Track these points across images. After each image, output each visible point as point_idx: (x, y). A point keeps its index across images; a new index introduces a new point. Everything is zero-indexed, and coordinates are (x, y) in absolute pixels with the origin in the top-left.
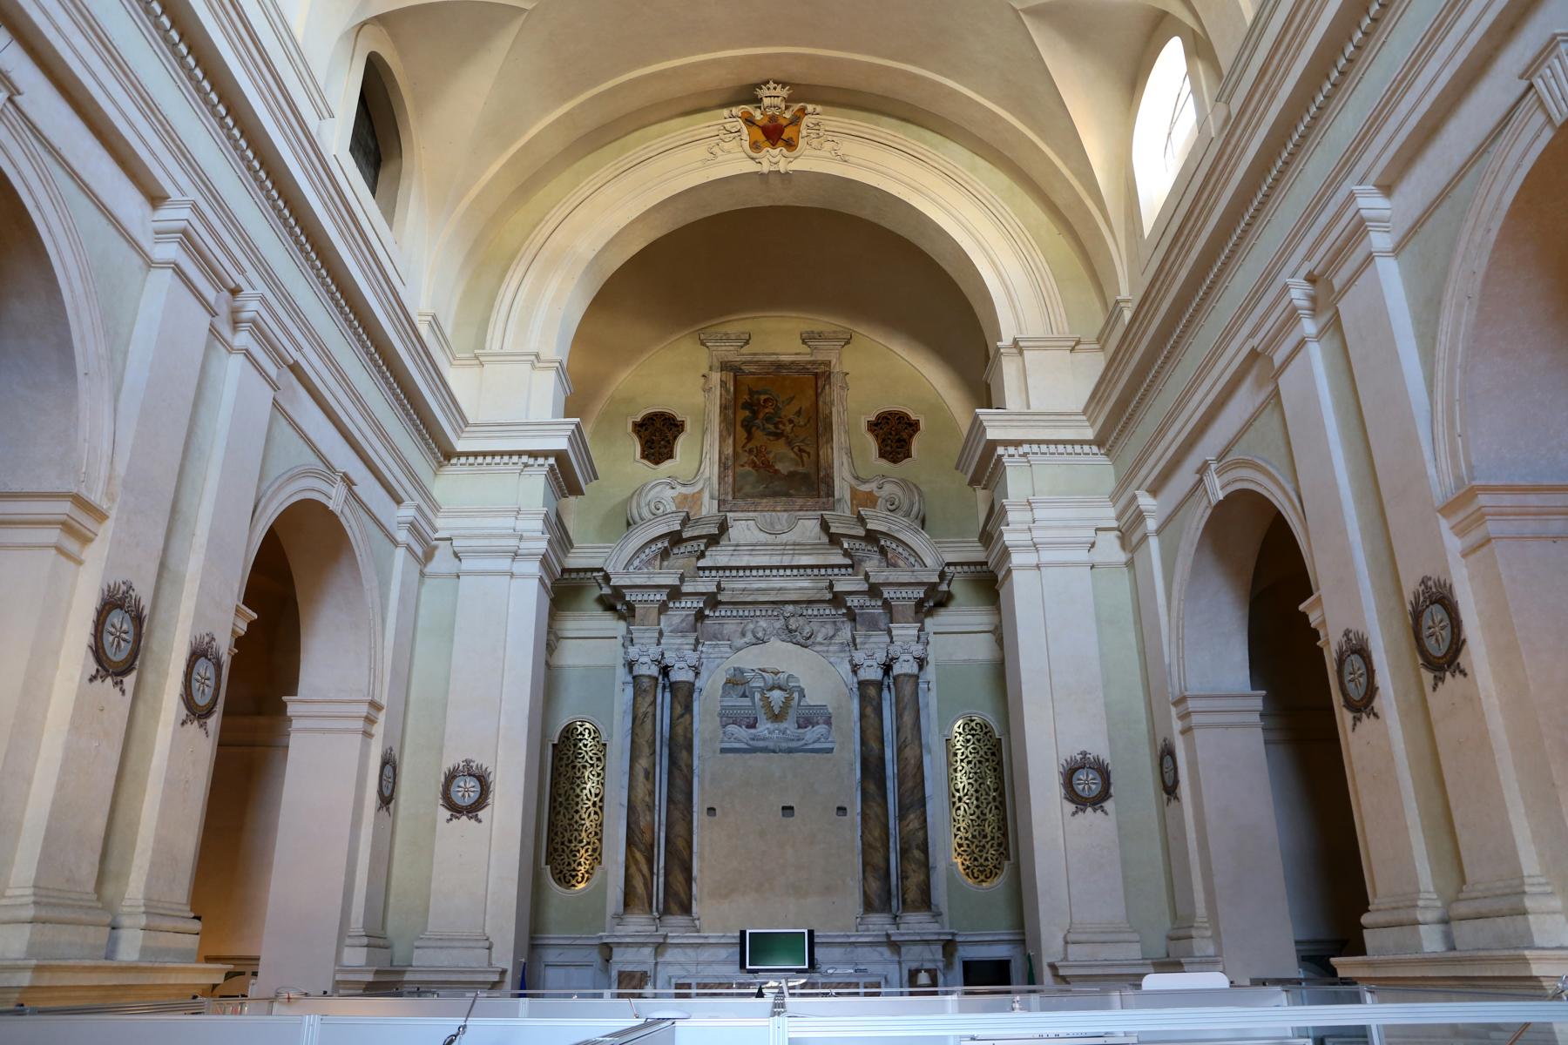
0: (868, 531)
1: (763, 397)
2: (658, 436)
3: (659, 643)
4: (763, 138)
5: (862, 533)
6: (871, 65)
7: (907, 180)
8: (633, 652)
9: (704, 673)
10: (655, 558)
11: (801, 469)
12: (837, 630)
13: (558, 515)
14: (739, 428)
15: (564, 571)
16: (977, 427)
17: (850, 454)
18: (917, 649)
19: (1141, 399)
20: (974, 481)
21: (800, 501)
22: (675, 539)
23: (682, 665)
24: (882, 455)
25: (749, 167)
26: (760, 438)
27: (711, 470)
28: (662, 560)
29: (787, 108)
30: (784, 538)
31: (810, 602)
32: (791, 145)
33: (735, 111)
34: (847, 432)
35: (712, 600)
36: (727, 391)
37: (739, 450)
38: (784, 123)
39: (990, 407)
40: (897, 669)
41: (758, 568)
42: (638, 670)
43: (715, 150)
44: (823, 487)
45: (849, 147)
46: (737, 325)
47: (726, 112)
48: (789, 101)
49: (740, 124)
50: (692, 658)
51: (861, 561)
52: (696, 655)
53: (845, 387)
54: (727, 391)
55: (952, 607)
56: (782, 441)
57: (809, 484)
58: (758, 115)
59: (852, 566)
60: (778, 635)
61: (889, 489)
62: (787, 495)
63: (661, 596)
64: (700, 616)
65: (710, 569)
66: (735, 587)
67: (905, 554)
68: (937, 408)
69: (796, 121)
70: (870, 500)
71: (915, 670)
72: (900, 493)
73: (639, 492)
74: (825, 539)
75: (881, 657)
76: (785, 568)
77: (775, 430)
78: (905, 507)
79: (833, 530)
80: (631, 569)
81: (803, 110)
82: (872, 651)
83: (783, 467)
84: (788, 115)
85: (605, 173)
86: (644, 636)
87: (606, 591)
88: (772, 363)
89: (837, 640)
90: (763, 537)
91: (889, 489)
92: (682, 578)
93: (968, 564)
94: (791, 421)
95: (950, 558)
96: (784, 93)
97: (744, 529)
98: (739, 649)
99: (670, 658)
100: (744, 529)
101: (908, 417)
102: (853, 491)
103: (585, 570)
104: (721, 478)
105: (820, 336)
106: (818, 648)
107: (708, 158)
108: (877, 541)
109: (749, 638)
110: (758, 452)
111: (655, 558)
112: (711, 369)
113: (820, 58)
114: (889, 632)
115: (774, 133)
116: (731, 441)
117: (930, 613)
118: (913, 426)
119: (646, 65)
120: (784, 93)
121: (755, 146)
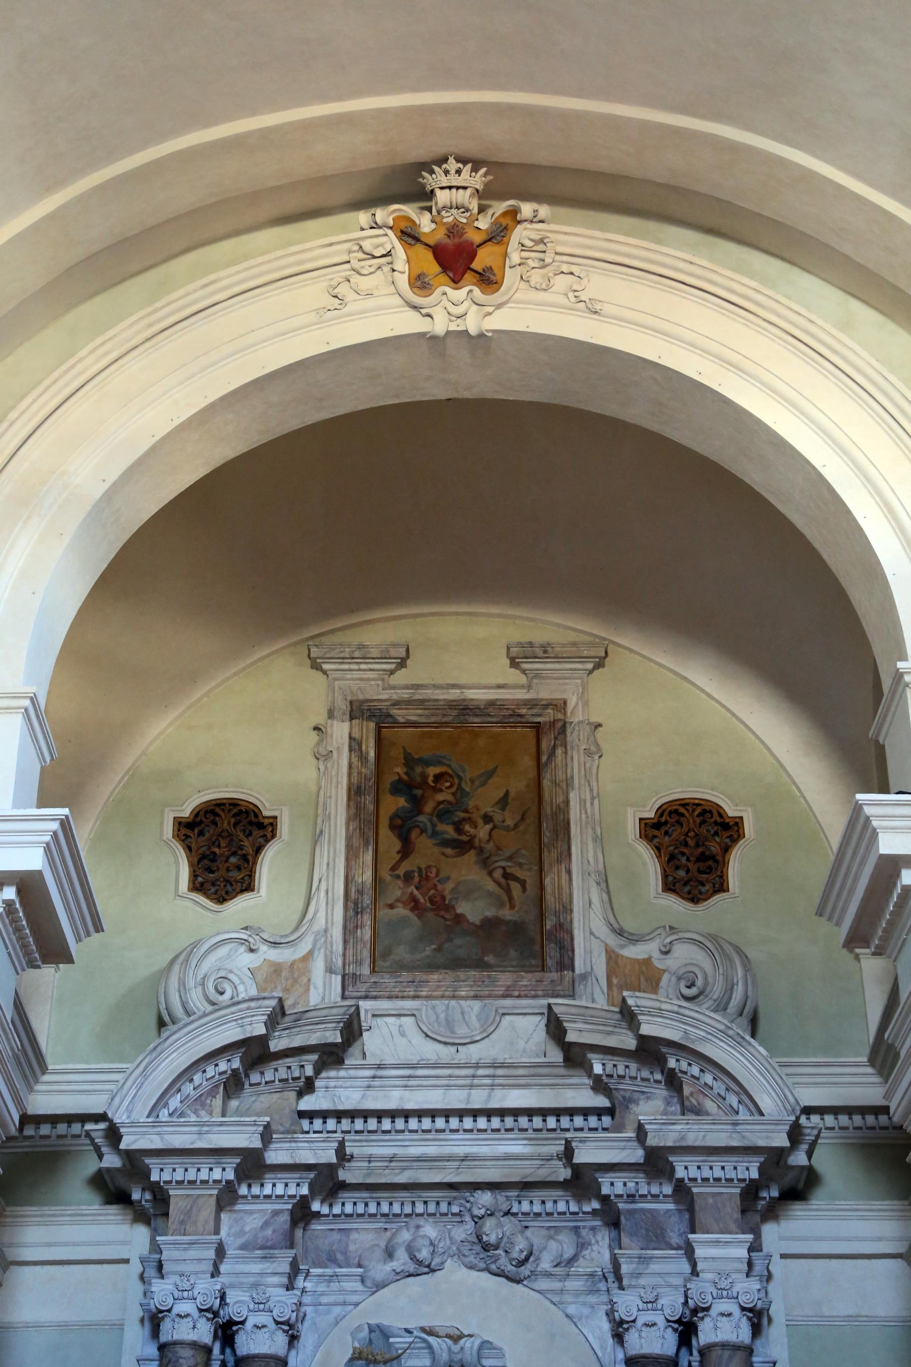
0: (643, 1040)
1: (433, 771)
2: (224, 844)
3: (215, 1273)
4: (435, 268)
5: (631, 1043)
6: (646, 126)
7: (714, 347)
8: (162, 1290)
9: (307, 1338)
10: (212, 1093)
11: (507, 914)
12: (582, 1246)
13: (18, 1006)
14: (385, 831)
15: (26, 1119)
16: (860, 830)
17: (604, 882)
18: (748, 1290)
19: (68, 903)
20: (856, 939)
21: (504, 979)
22: (255, 1053)
23: (263, 1318)
24: (669, 887)
25: (408, 323)
26: (426, 850)
27: (329, 913)
28: (228, 1096)
29: (482, 209)
30: (474, 1052)
31: (526, 1186)
32: (488, 281)
33: (383, 214)
34: (599, 840)
35: (328, 1181)
36: (363, 758)
37: (386, 875)
38: (477, 238)
39: (885, 790)
40: (708, 1332)
41: (420, 1114)
42: (171, 1331)
43: (343, 290)
44: (551, 950)
45: (600, 285)
46: (382, 630)
47: (363, 217)
48: (485, 195)
49: (392, 240)
50: (283, 1303)
51: (629, 1101)
52: (291, 1298)
53: (594, 752)
54: (363, 758)
55: (818, 1201)
56: (471, 857)
57: (523, 942)
58: (425, 224)
59: (610, 1112)
60: (460, 1255)
61: (685, 955)
62: (480, 965)
63: (224, 1172)
64: (302, 1214)
65: (324, 1115)
66: (373, 1152)
67: (719, 1088)
68: (780, 793)
69: (498, 235)
70: (647, 977)
71: (744, 1334)
72: (706, 964)
73: (184, 957)
74: (556, 1056)
75: (672, 1304)
76: (475, 1114)
77: (458, 837)
78: (717, 991)
79: (571, 1037)
80: (164, 1115)
81: (513, 213)
82: (656, 1289)
83: (473, 910)
84: (484, 223)
85: (128, 331)
86: (187, 1256)
87: (112, 1161)
88: (451, 705)
89: (582, 1267)
90: (431, 1051)
91: (685, 955)
92: (267, 1135)
93: (849, 1111)
94: (487, 819)
95: (811, 1096)
96: (478, 180)
97: (393, 1034)
98: (380, 1286)
99: (238, 1304)
100: (393, 1034)
101: (721, 813)
102: (612, 958)
103: (70, 1119)
104: (349, 931)
105: (546, 652)
106: (543, 1284)
107: (327, 306)
108: (659, 1061)
109: (401, 1260)
110: (423, 878)
111: (212, 1093)
112: (331, 715)
113: (545, 112)
114: (689, 1251)
115: (456, 259)
116: (369, 857)
117: (772, 1213)
118: (732, 830)
119: (207, 124)
120: (478, 180)
121: (420, 283)
